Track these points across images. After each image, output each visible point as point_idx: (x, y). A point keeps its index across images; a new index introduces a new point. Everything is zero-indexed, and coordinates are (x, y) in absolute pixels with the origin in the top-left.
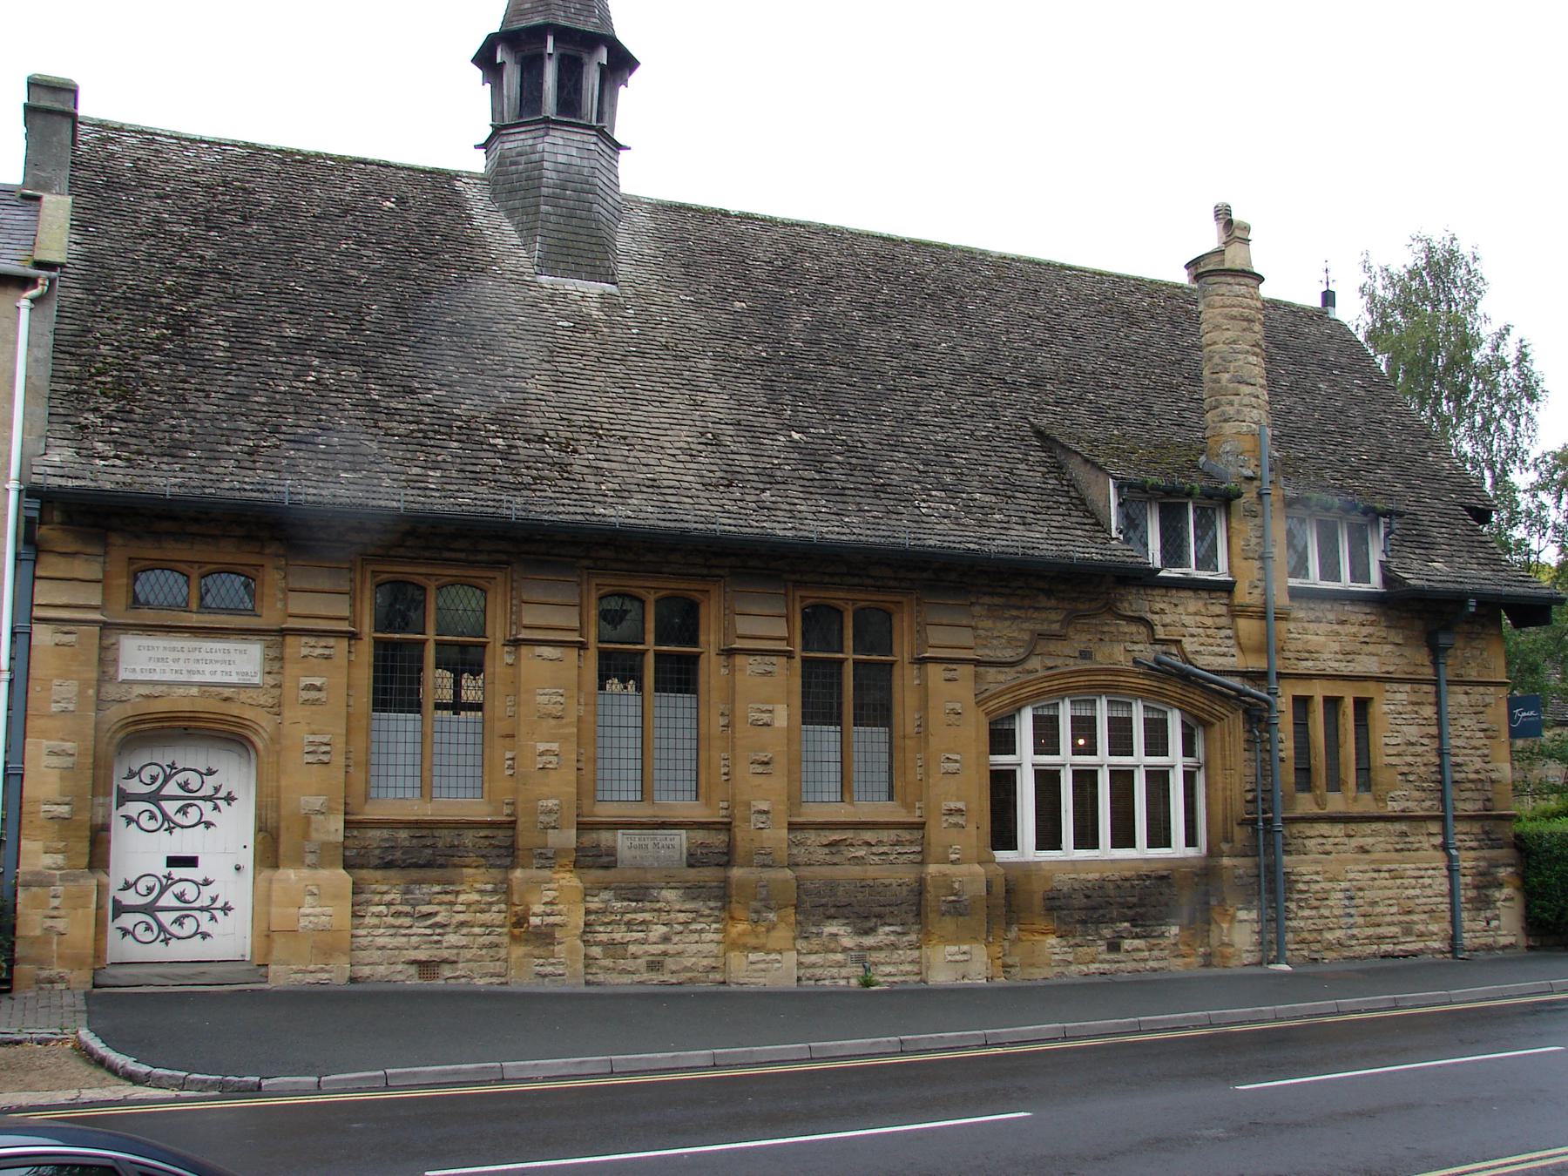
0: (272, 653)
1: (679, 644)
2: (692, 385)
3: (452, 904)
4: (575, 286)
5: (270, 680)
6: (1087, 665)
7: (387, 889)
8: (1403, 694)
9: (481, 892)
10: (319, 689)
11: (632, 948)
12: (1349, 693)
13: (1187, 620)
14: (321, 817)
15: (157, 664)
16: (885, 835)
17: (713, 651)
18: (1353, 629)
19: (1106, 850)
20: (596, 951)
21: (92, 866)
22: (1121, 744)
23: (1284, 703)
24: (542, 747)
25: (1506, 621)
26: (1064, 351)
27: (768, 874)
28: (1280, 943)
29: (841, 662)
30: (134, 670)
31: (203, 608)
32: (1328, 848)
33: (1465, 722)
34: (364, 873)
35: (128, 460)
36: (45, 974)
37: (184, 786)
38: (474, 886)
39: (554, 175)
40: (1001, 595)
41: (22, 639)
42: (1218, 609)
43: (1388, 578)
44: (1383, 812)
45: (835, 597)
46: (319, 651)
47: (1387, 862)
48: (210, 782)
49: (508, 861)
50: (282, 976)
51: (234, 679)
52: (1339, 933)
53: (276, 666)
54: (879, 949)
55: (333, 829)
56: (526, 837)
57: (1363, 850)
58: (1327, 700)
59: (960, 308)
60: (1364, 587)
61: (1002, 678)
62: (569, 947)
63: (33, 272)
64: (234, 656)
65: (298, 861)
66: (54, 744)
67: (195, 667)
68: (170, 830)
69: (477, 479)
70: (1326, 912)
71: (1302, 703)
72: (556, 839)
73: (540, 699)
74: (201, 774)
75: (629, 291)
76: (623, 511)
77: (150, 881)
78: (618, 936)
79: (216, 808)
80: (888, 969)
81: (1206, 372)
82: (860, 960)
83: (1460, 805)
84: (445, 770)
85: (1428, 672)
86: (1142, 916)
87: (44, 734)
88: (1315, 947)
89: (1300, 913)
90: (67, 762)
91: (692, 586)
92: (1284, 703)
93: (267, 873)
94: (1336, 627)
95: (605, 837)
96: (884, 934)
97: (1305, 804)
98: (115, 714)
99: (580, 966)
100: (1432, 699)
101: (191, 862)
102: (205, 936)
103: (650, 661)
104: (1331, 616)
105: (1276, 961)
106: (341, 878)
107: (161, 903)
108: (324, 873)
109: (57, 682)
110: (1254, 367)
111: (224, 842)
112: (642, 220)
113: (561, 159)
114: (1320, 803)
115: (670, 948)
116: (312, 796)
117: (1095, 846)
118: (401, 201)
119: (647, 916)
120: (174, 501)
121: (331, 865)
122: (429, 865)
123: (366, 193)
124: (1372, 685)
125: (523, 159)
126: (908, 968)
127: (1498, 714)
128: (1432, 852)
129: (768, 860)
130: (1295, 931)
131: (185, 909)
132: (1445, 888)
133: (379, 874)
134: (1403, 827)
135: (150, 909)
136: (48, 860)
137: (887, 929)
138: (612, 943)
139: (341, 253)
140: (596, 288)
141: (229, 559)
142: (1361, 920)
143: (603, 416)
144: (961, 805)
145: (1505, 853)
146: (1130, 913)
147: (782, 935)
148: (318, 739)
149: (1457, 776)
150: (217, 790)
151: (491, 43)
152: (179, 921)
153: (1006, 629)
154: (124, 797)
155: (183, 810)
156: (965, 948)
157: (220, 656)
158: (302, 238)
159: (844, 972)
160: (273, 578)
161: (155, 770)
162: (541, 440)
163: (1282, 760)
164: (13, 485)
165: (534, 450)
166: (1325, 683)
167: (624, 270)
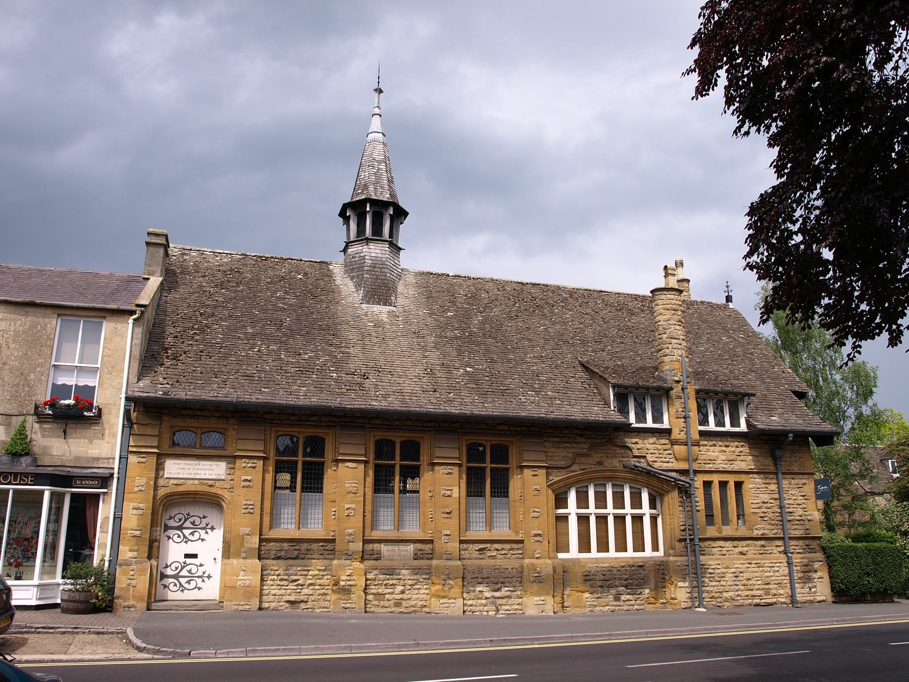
1: (411, 460)
2: (424, 349)
3: (306, 575)
4: (376, 308)
5: (230, 477)
7: (277, 568)
9: (319, 570)
10: (250, 481)
11: (387, 596)
12: (731, 479)
13: (649, 446)
15: (179, 470)
16: (508, 546)
17: (426, 464)
20: (370, 597)
21: (149, 557)
24: (347, 506)
26: (598, 328)
28: (701, 599)
29: (485, 468)
31: (201, 447)
32: (724, 552)
34: (268, 562)
36: (127, 604)
38: (316, 566)
40: (558, 437)
41: (124, 460)
42: (663, 441)
43: (749, 424)
45: (482, 439)
46: (250, 465)
47: (757, 559)
51: (214, 477)
52: (731, 594)
53: (232, 471)
54: (503, 598)
56: (339, 546)
57: (742, 553)
58: (720, 482)
59: (552, 312)
60: (736, 429)
63: (134, 308)
64: (214, 467)
65: (238, 556)
66: (136, 505)
67: (197, 472)
68: (186, 542)
70: (724, 584)
71: (707, 485)
72: (352, 546)
75: (401, 310)
76: (384, 403)
77: (177, 565)
78: (380, 591)
80: (507, 607)
82: (493, 603)
83: (793, 532)
85: (772, 468)
86: (631, 584)
87: (131, 500)
88: (719, 600)
89: (711, 584)
90: (140, 512)
91: (416, 435)
93: (226, 561)
95: (376, 546)
96: (504, 591)
97: (711, 532)
98: (161, 492)
99: (363, 604)
101: (195, 556)
104: (720, 443)
105: (699, 606)
106: (256, 563)
108: (249, 561)
110: (679, 331)
111: (209, 545)
112: (411, 279)
114: (720, 531)
115: (405, 596)
116: (246, 527)
117: (608, 551)
118: (305, 274)
119: (394, 582)
120: (187, 401)
121: (253, 558)
122: (296, 558)
123: (291, 272)
126: (516, 607)
128: (778, 555)
129: (450, 557)
130: (708, 592)
131: (191, 577)
132: (786, 572)
133: (274, 562)
134: (763, 542)
135: (176, 577)
136: (130, 554)
137: (506, 589)
138: (378, 594)
140: (387, 308)
141: (213, 426)
142: (742, 587)
143: (382, 363)
144: (540, 532)
145: (820, 555)
146: (625, 582)
147: (456, 591)
148: (249, 503)
149: (790, 518)
150: (207, 525)
151: (345, 207)
153: (562, 453)
154: (167, 528)
156: (543, 598)
157: (208, 467)
158: (261, 292)
159: (486, 608)
160: (232, 433)
161: (181, 516)
163: (698, 511)
164: (123, 396)
165: (349, 378)
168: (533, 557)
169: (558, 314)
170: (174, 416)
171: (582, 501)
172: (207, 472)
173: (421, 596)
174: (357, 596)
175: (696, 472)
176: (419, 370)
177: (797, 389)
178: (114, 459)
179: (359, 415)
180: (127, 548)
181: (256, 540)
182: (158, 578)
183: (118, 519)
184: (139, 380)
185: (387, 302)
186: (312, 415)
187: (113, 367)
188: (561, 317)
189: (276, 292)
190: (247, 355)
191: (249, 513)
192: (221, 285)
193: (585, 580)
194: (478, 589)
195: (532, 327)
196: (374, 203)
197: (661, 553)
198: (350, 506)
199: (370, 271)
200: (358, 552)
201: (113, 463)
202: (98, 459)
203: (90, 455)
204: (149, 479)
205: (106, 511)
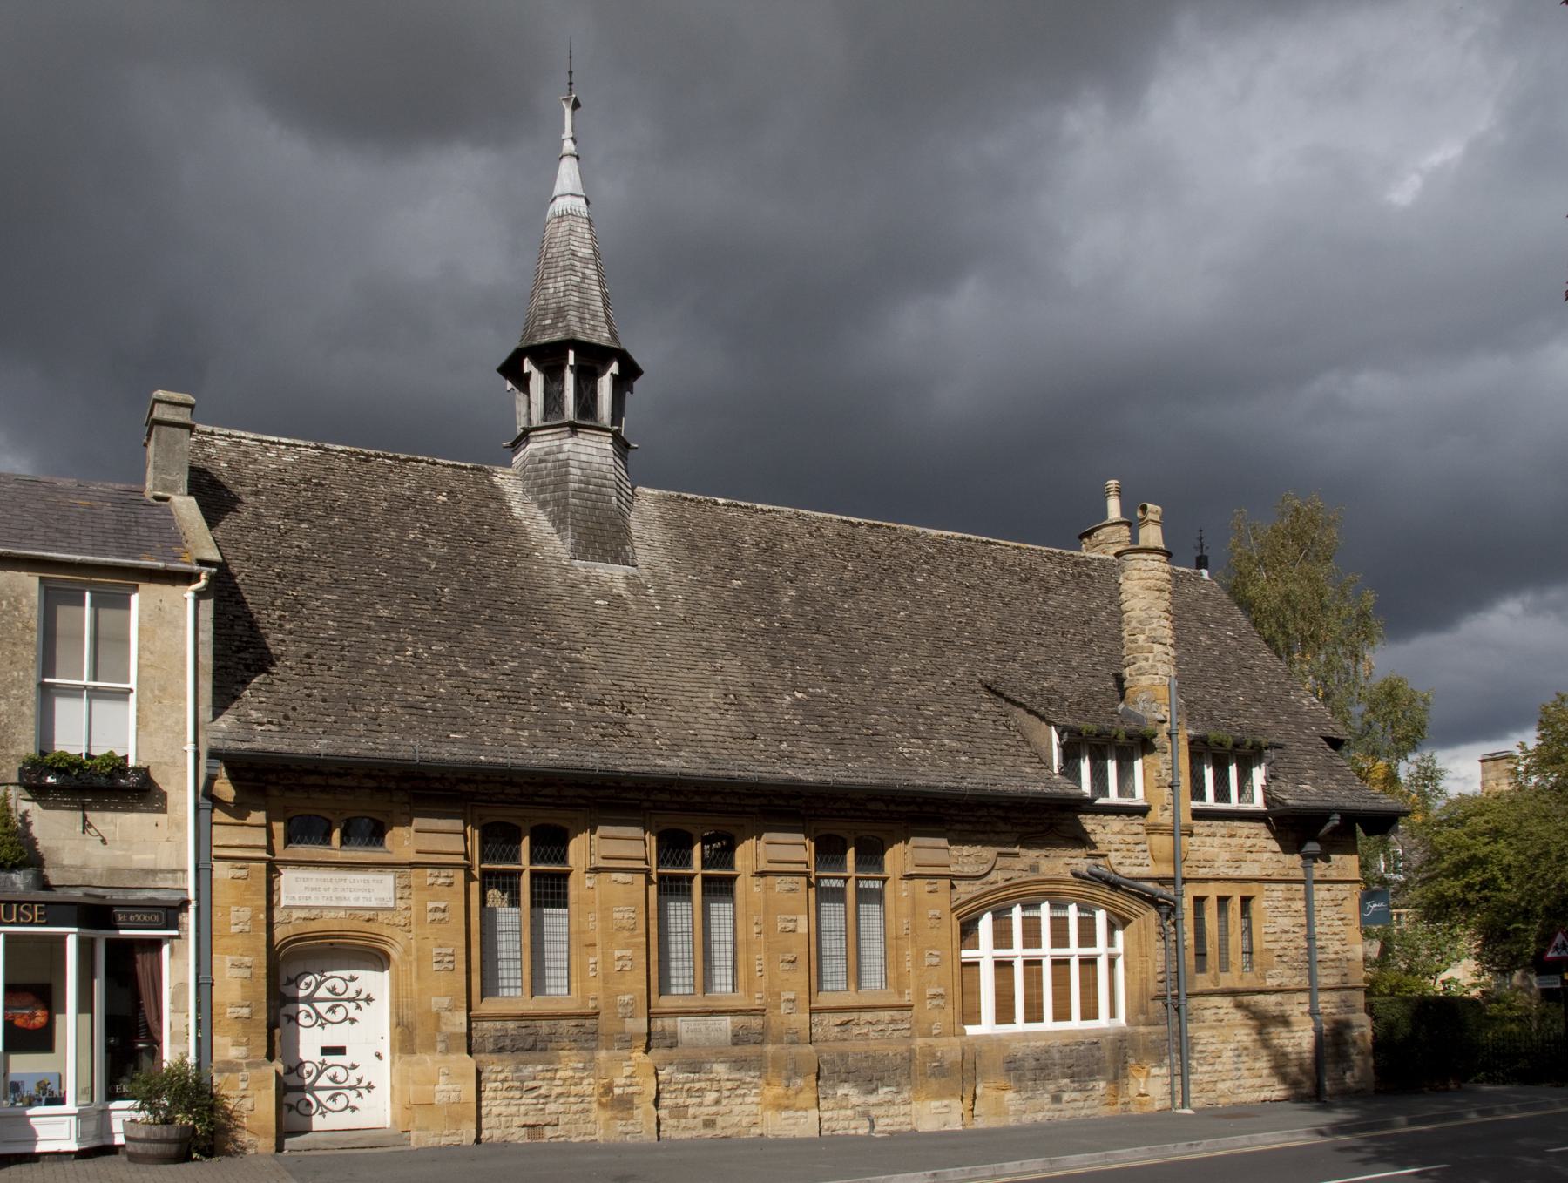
0: (403, 882)
2: (710, 654)
4: (603, 570)
6: (1033, 876)
7: (499, 1069)
8: (1279, 891)
9: (574, 1069)
11: (691, 1111)
12: (1236, 892)
18: (1241, 841)
19: (1049, 1024)
20: (663, 1113)
21: (271, 1056)
22: (1060, 939)
23: (1187, 903)
24: (618, 954)
25: (1361, 833)
27: (795, 1049)
33: (1327, 913)
34: (482, 1056)
35: (280, 724)
37: (332, 990)
38: (569, 1063)
39: (579, 472)
40: (969, 822)
44: (1263, 987)
46: (441, 881)
48: (353, 986)
49: (593, 1044)
50: (421, 1138)
51: (374, 904)
52: (1228, 1084)
53: (407, 892)
56: (605, 1024)
61: (970, 888)
62: (644, 1113)
63: (196, 568)
65: (430, 1047)
67: (339, 894)
68: (322, 1025)
69: (558, 736)
71: (1199, 901)
73: (616, 915)
78: (680, 1101)
79: (358, 1007)
80: (887, 1121)
81: (1125, 634)
82: (866, 1115)
84: (512, 974)
87: (227, 950)
88: (1211, 1095)
90: (247, 973)
92: (1187, 903)
94: (1228, 840)
95: (668, 1023)
96: (883, 1093)
97: (1203, 982)
99: (654, 1125)
100: (1301, 895)
101: (340, 1051)
102: (354, 1109)
103: (525, 881)
104: (1224, 831)
106: (468, 1064)
107: (318, 1084)
108: (453, 1057)
109: (234, 908)
110: (1163, 628)
113: (583, 458)
114: (1216, 980)
117: (1040, 1020)
118: (451, 493)
119: (703, 1085)
121: (458, 1050)
122: (532, 1049)
123: (420, 490)
124: (1255, 885)
125: (551, 458)
126: (902, 1119)
127: (1351, 908)
131: (337, 1088)
133: (494, 1057)
137: (886, 1089)
138: (677, 1107)
139: (410, 543)
140: (620, 571)
142: (1246, 1073)
143: (645, 682)
144: (941, 991)
147: (808, 1096)
148: (444, 951)
156: (945, 1102)
158: (377, 530)
162: (601, 703)
166: (1218, 884)
167: (643, 554)
168: (930, 1035)
169: (923, 586)
170: (290, 788)
171: (1002, 937)
172: (361, 895)
173: (747, 1108)
174: (644, 1113)
175: (1185, 881)
176: (712, 697)
177: (1330, 733)
178: (185, 871)
179: (629, 784)
180: (228, 1040)
181: (461, 1017)
182: (292, 1096)
183: (204, 985)
184: (216, 715)
185: (619, 557)
186: (545, 785)
187: (163, 689)
188: (930, 592)
189: (404, 529)
190: (396, 663)
192: (296, 514)
193: (1008, 1070)
194: (840, 1092)
195: (886, 613)
196: (583, 348)
197: (1121, 1019)
198: (624, 953)
199: (580, 490)
200: (638, 1035)
201: (185, 880)
202: (153, 872)
203: (135, 865)
204: (256, 910)
205: (175, 971)
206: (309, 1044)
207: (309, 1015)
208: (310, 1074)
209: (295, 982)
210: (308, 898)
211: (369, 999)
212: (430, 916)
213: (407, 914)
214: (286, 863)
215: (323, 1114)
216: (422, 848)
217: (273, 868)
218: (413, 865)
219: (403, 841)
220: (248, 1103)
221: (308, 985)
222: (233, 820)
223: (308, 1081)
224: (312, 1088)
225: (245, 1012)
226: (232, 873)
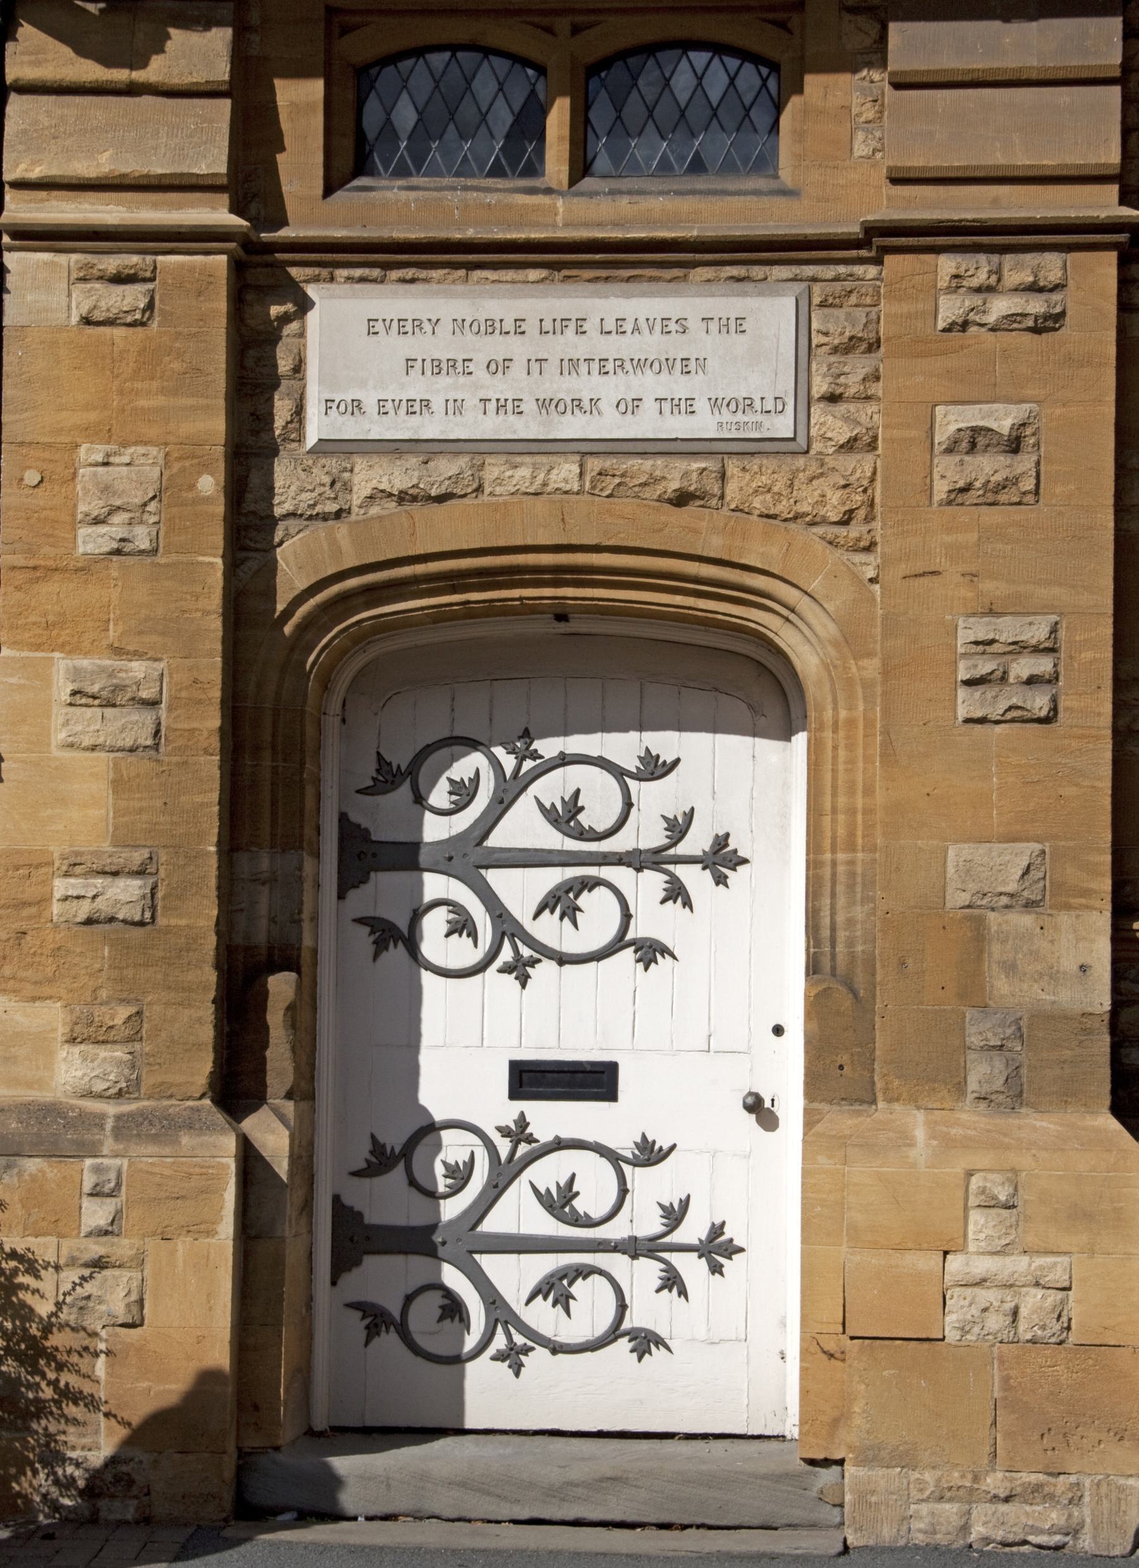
0: (837, 325)
14: (1025, 920)
21: (236, 1087)
30: (357, 405)
37: (566, 815)
46: (1000, 307)
48: (655, 800)
51: (704, 425)
53: (857, 367)
55: (1069, 964)
65: (939, 1077)
67: (563, 387)
68: (520, 970)
74: (619, 773)
79: (676, 893)
90: (135, 726)
93: (842, 1120)
101: (595, 1081)
102: (646, 1343)
107: (495, 1223)
108: (1039, 1124)
109: (90, 452)
121: (1067, 1095)
131: (577, 1248)
148: (1008, 629)
152: (556, 1289)
155: (562, 902)
172: (649, 385)
191: (1019, 717)
204: (182, 457)
206: (464, 1044)
207: (462, 925)
208: (460, 1176)
209: (405, 778)
210: (420, 407)
211: (722, 859)
212: (948, 474)
213: (860, 465)
214: (332, 255)
215: (513, 1357)
216: (918, 160)
217: (263, 280)
218: (881, 240)
219: (846, 139)
220: (113, 1294)
221: (464, 793)
222: (91, 71)
223: (451, 1209)
224: (473, 1242)
225: (125, 894)
226: (82, 300)
